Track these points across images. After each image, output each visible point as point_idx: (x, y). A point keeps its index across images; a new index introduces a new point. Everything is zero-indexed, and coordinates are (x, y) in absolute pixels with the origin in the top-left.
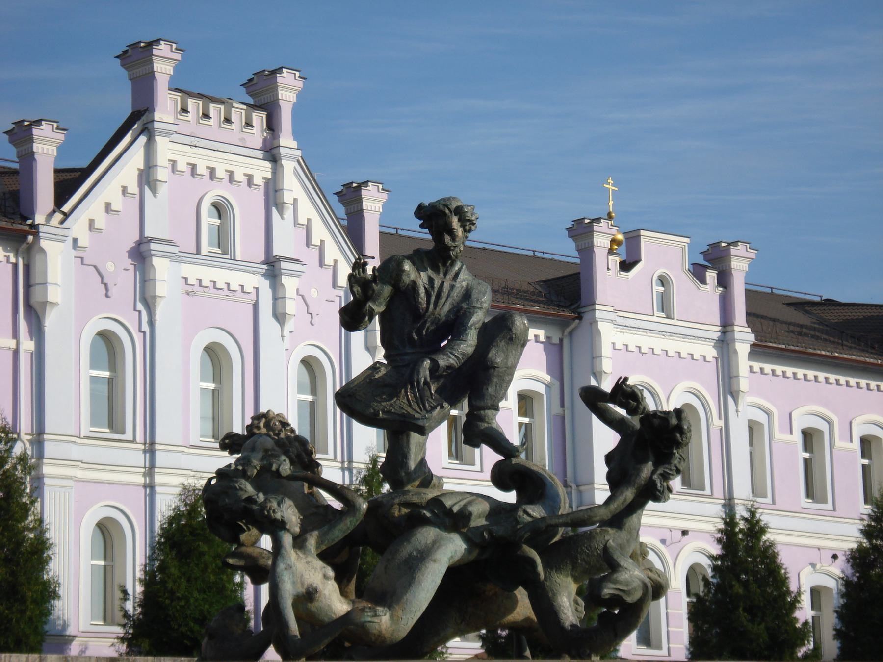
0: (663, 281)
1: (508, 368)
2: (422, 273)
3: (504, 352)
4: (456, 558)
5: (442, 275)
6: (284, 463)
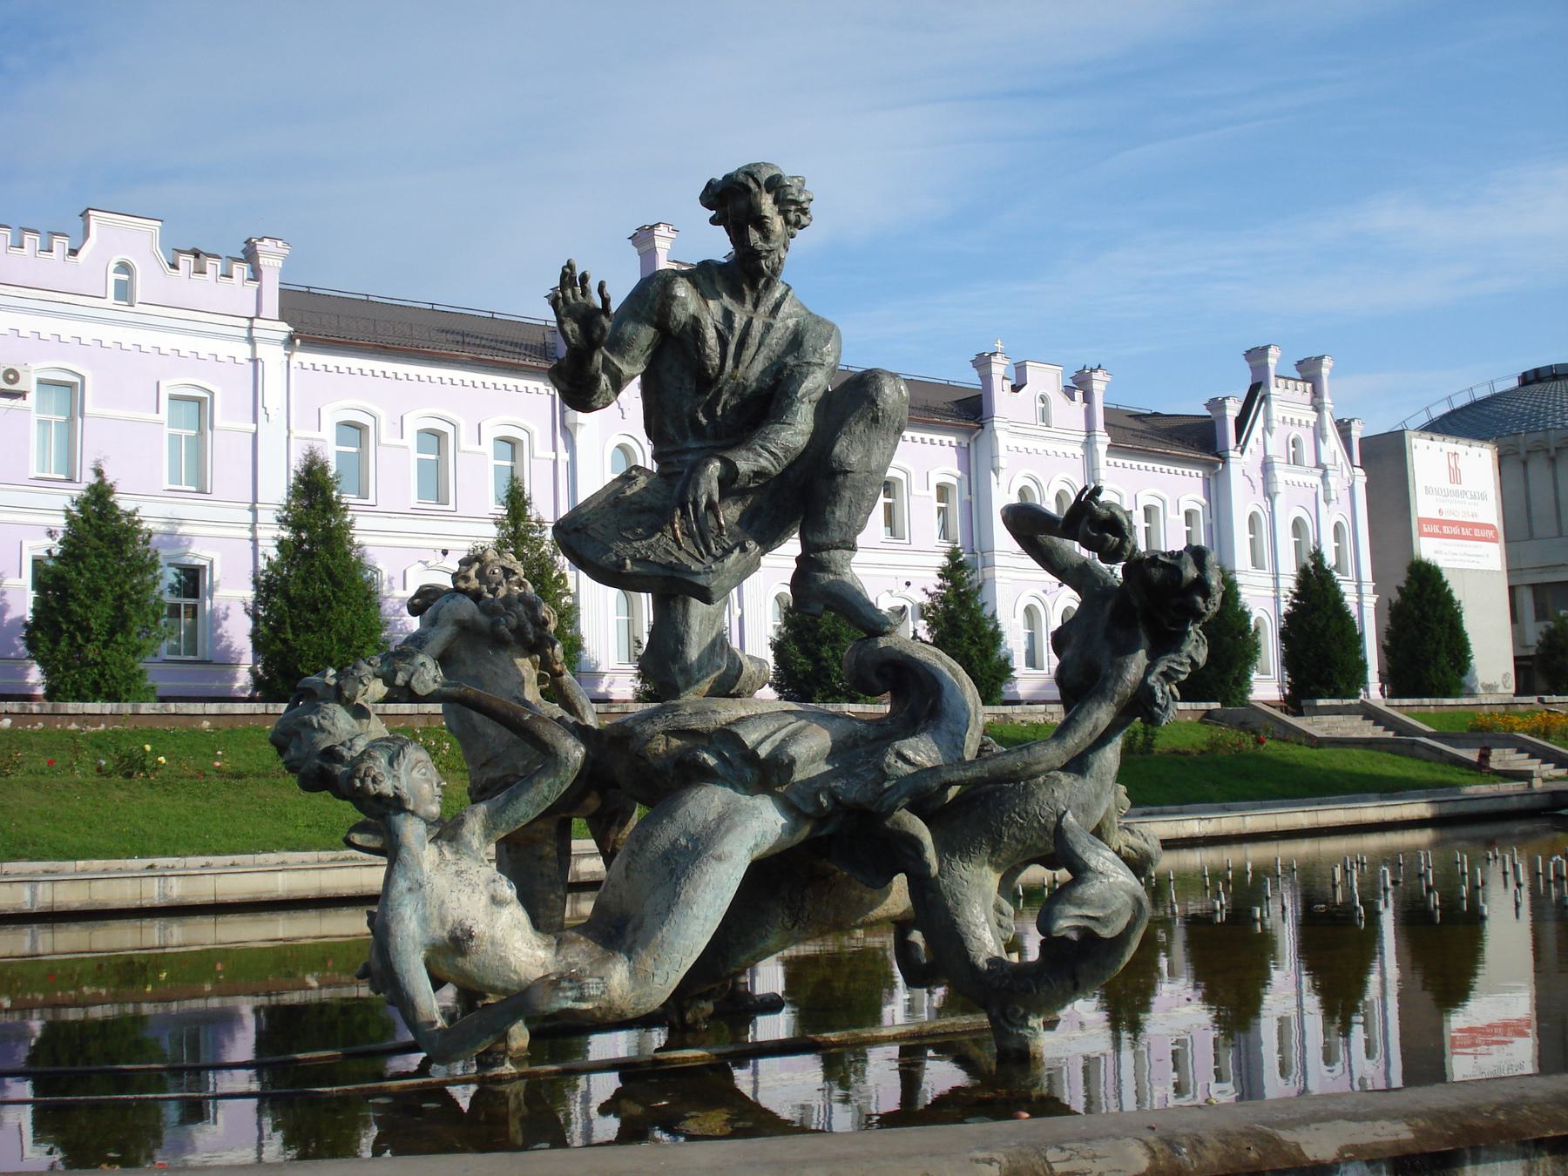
0: (1043, 399)
1: (870, 472)
2: (711, 303)
3: (862, 442)
4: (765, 847)
5: (749, 306)
6: (422, 669)
